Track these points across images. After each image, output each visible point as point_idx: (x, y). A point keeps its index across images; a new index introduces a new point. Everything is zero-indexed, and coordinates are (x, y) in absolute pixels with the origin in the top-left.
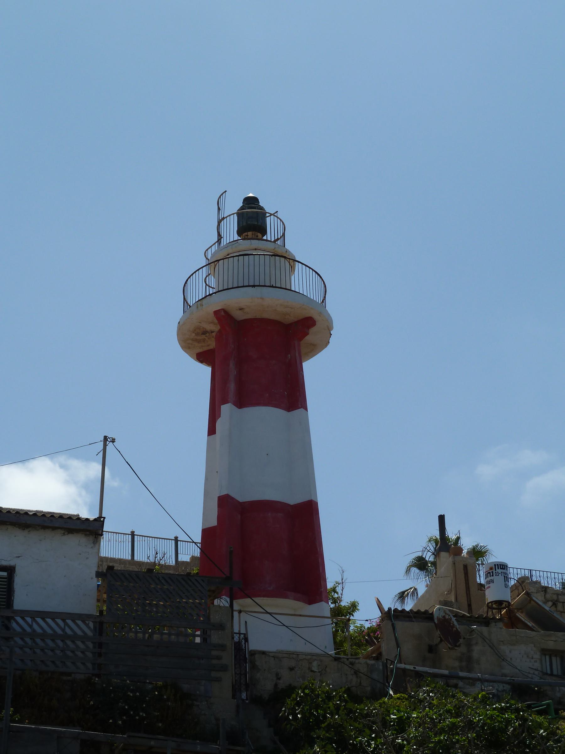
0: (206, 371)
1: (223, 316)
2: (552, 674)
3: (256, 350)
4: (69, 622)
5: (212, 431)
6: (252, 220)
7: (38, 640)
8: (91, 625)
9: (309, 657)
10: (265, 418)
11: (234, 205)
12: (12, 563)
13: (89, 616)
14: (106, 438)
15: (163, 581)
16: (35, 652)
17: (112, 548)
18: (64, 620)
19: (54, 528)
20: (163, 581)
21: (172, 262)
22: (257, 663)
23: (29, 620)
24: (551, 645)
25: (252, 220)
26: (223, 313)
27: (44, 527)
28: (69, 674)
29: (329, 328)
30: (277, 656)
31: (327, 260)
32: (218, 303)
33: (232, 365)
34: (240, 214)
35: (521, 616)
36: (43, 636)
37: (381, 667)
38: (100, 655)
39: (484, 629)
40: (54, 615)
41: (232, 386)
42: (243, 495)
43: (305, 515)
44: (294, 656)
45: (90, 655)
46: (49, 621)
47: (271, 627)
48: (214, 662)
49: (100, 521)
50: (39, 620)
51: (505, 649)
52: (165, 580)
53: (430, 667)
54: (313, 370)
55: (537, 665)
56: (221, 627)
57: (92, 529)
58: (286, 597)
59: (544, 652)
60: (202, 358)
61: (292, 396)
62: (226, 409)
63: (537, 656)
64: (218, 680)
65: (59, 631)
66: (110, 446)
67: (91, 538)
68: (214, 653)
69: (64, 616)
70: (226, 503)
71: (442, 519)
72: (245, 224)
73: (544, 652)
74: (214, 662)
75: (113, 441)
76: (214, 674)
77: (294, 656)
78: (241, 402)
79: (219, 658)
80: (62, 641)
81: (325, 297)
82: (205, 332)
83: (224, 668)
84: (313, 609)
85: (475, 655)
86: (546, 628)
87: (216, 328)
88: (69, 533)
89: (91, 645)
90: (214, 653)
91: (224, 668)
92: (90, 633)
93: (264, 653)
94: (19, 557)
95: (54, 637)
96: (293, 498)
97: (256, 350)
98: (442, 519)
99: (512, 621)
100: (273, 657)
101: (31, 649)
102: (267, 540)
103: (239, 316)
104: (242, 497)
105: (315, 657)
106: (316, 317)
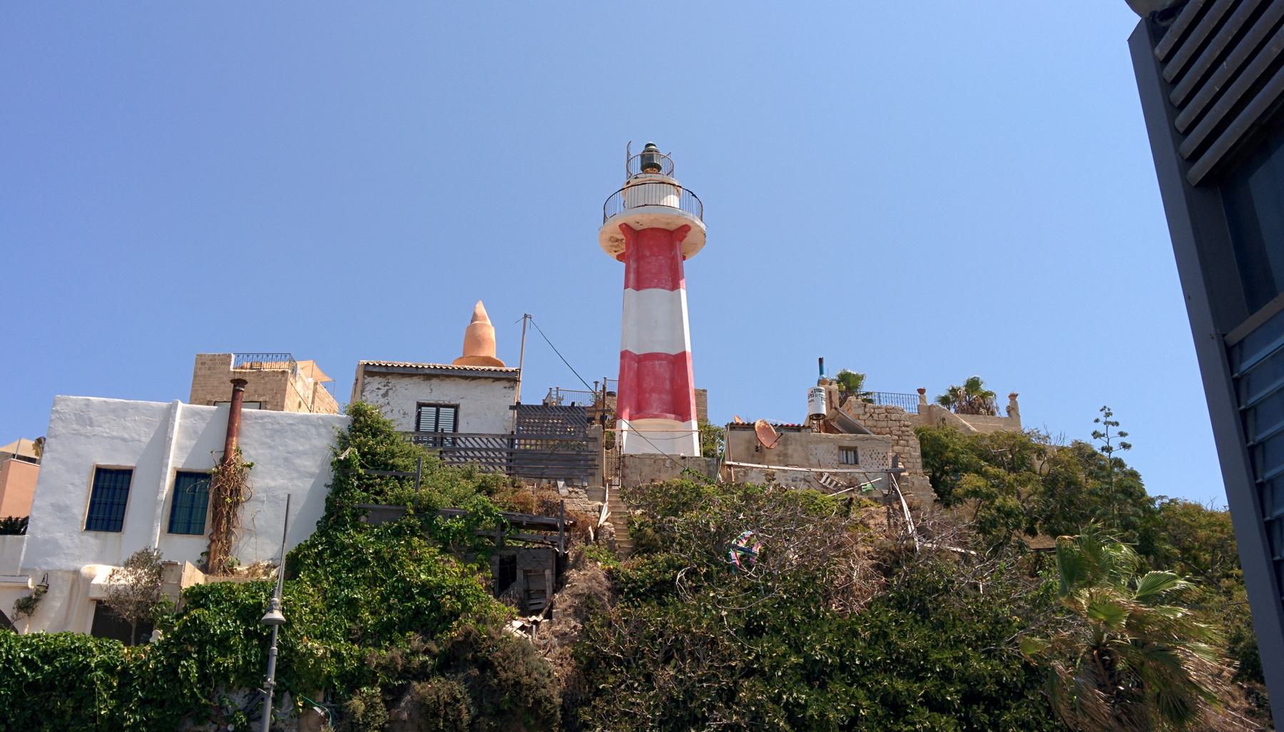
0: (623, 265)
6: (649, 163)
10: (657, 295)
11: (638, 150)
13: (503, 436)
24: (846, 444)
25: (649, 163)
27: (466, 378)
35: (834, 424)
40: (480, 436)
41: (632, 276)
54: (687, 266)
63: (836, 451)
64: (593, 475)
71: (821, 360)
73: (841, 448)
87: (621, 236)
96: (674, 351)
97: (654, 254)
98: (821, 360)
99: (828, 428)
102: (658, 382)
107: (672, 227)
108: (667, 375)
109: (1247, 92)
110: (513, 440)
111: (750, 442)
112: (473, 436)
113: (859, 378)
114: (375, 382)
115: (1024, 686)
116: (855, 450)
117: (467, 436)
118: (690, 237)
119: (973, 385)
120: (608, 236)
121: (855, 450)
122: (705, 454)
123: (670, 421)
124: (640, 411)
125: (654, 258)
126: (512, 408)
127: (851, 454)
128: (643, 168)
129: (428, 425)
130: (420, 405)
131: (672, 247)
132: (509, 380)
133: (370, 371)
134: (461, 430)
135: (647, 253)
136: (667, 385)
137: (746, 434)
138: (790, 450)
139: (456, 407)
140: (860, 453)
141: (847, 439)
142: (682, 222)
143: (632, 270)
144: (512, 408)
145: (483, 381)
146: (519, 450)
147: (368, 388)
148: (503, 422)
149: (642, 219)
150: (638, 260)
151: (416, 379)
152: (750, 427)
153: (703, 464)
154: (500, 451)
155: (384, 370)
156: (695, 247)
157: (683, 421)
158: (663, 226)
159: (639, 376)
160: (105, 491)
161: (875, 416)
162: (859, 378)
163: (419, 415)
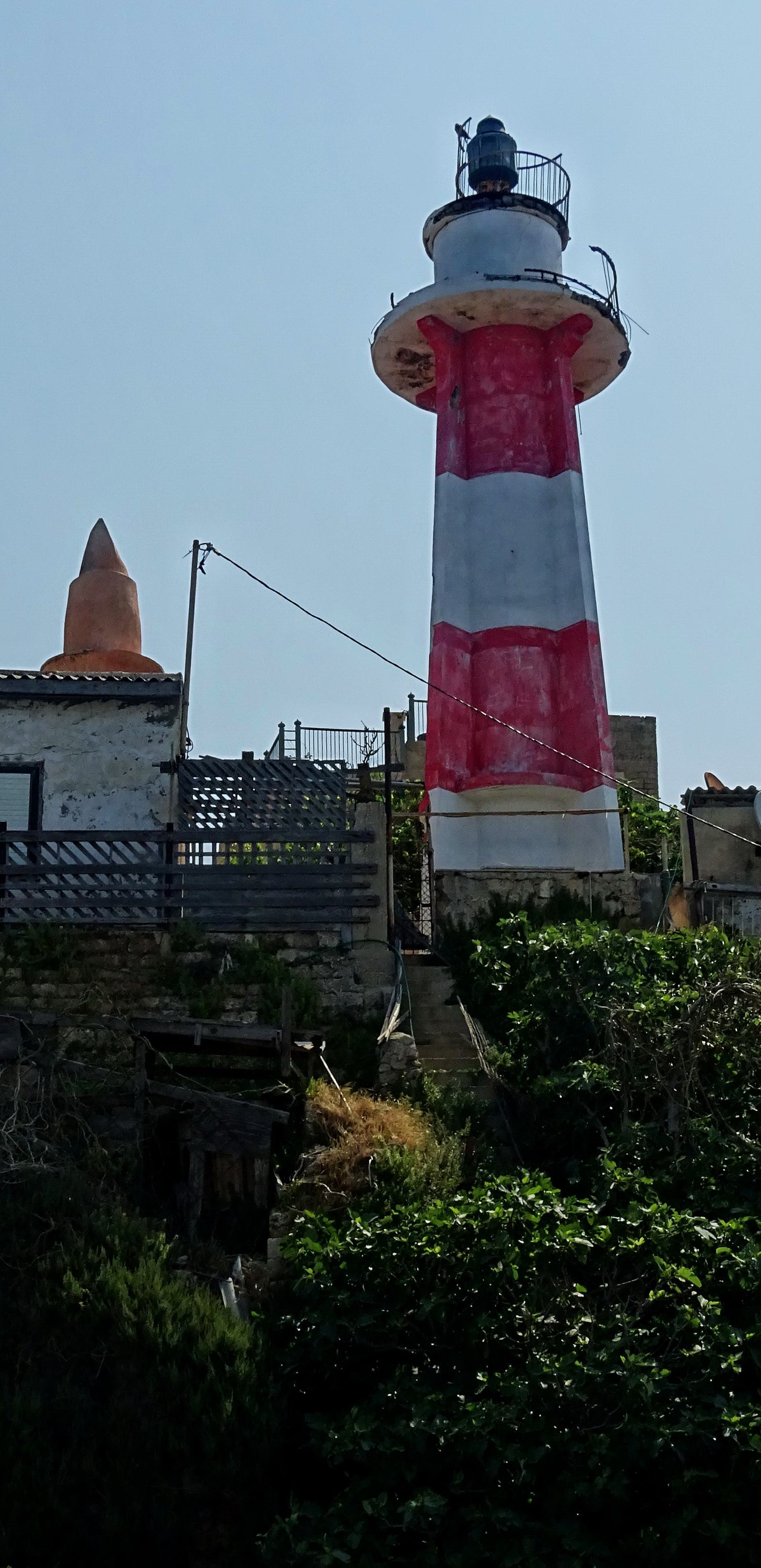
0: (732, 788)
3: (503, 364)
4: (119, 845)
6: (490, 159)
7: (68, 877)
9: (534, 875)
12: (38, 758)
14: (196, 545)
15: (271, 770)
16: (63, 895)
18: (109, 843)
19: (105, 698)
20: (271, 770)
22: (445, 890)
25: (490, 159)
26: (430, 323)
27: (54, 699)
29: (380, 338)
37: (659, 885)
43: (576, 645)
44: (508, 875)
45: (151, 893)
46: (86, 845)
48: (356, 893)
50: (70, 845)
52: (276, 769)
53: (394, 869)
60: (424, 401)
61: (557, 453)
64: (364, 921)
65: (102, 860)
66: (211, 561)
68: (358, 879)
70: (443, 634)
72: (477, 167)
74: (356, 893)
76: (356, 912)
77: (508, 875)
79: (364, 886)
80: (108, 875)
81: (581, 284)
82: (415, 358)
83: (374, 902)
84: (585, 800)
88: (130, 704)
90: (358, 879)
91: (374, 902)
93: (457, 873)
94: (50, 748)
96: (557, 621)
97: (503, 364)
100: (473, 879)
101: (57, 891)
105: (543, 875)
107: (548, 321)
108: (543, 684)
109: (691, 851)
112: (76, 836)
113: (252, 753)
117: (61, 837)
118: (590, 348)
120: (394, 350)
122: (636, 864)
123: (548, 793)
125: (503, 400)
126: (166, 767)
131: (548, 370)
132: (160, 701)
134: (51, 821)
135: (488, 386)
136: (544, 703)
140: (48, 786)
144: (166, 767)
151: (95, 703)
153: (629, 889)
154: (142, 870)
159: (477, 691)
162: (252, 753)
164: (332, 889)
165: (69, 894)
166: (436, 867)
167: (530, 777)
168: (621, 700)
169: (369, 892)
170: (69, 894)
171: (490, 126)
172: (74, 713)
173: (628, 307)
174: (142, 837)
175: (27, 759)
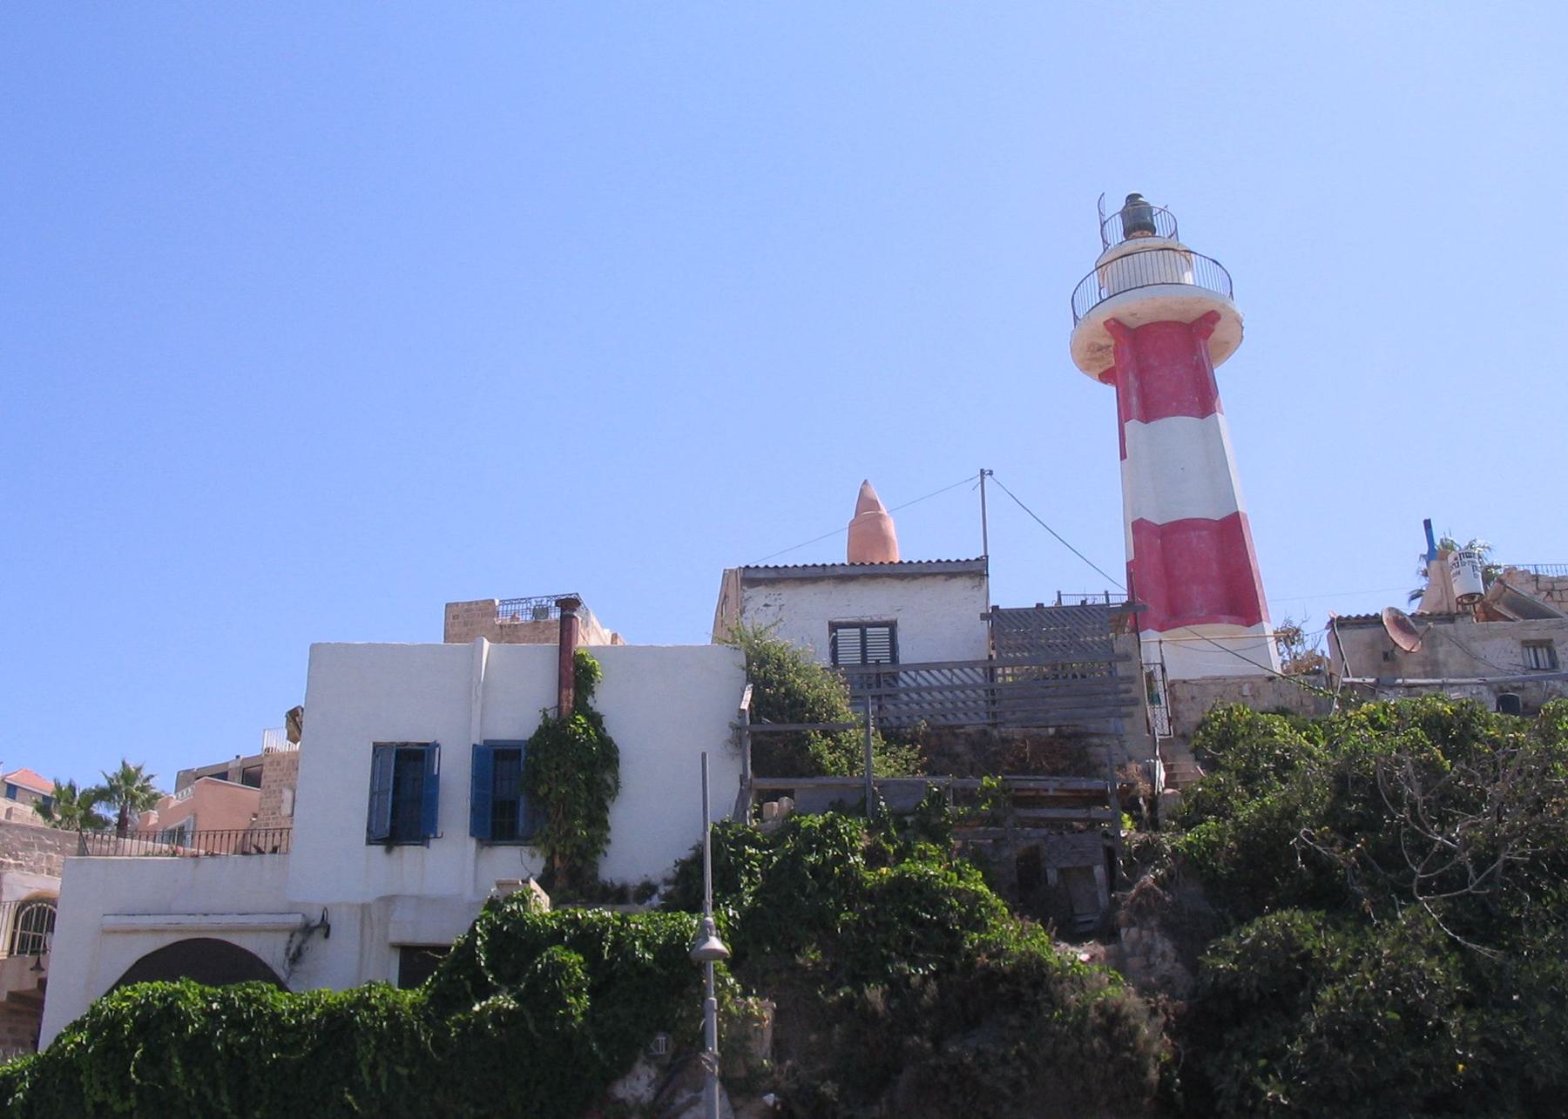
0: (1110, 391)
1: (1116, 326)
2: (1538, 668)
3: (1162, 362)
5: (1123, 456)
6: (1137, 218)
8: (980, 671)
10: (1178, 428)
14: (982, 472)
17: (1012, 590)
19: (934, 575)
21: (1054, 280)
23: (913, 674)
24: (1533, 635)
25: (1137, 218)
27: (924, 575)
28: (962, 727)
30: (1202, 684)
31: (1227, 248)
32: (1106, 312)
33: (1131, 378)
34: (1124, 214)
36: (930, 689)
38: (994, 702)
39: (1449, 627)
40: (939, 666)
41: (1134, 400)
42: (1157, 516)
43: (1230, 530)
46: (935, 672)
47: (1187, 655)
49: (983, 561)
50: (924, 673)
51: (1476, 646)
54: (1225, 375)
55: (1519, 660)
56: (1127, 657)
57: (975, 571)
58: (1219, 621)
59: (1526, 644)
60: (1106, 377)
61: (1203, 400)
62: (1133, 426)
63: (1518, 649)
64: (1130, 715)
65: (946, 682)
66: (987, 478)
67: (977, 580)
68: (1122, 687)
69: (951, 666)
70: (1139, 528)
71: (1428, 524)
73: (1526, 644)
75: (991, 473)
76: (1124, 710)
78: (1147, 416)
79: (1127, 691)
82: (1100, 349)
85: (1441, 657)
86: (1526, 617)
89: (982, 692)
90: (1122, 687)
92: (980, 681)
95: (941, 689)
96: (1216, 514)
97: (1162, 362)
98: (1428, 524)
99: (1490, 615)
102: (1198, 565)
103: (1133, 323)
104: (1157, 519)
106: (1216, 308)
110: (992, 670)
111: (1372, 645)
112: (927, 667)
114: (759, 596)
115: (913, 742)
116: (1547, 644)
117: (917, 667)
118: (1220, 332)
119: (128, 776)
121: (1547, 644)
124: (1175, 616)
126: (984, 617)
127: (1543, 654)
128: (1128, 233)
129: (850, 655)
130: (834, 627)
131: (1193, 348)
133: (752, 578)
137: (1365, 634)
138: (1441, 653)
139: (892, 626)
140: (1558, 650)
141: (1536, 630)
142: (1208, 307)
143: (1133, 391)
144: (984, 617)
145: (929, 581)
146: (1005, 684)
147: (750, 606)
148: (973, 642)
149: (1137, 307)
150: (1141, 374)
152: (1376, 620)
155: (773, 574)
156: (1226, 349)
157: (1249, 625)
158: (1175, 318)
160: (203, 837)
161: (1556, 595)
163: (834, 643)
164: (1106, 694)
165: (926, 706)
166: (1171, 676)
167: (1211, 618)
168: (426, 629)
169: (1132, 695)
170: (926, 706)
171: (1133, 199)
172: (904, 583)
173: (1239, 306)
174: (972, 665)
175: (885, 618)
